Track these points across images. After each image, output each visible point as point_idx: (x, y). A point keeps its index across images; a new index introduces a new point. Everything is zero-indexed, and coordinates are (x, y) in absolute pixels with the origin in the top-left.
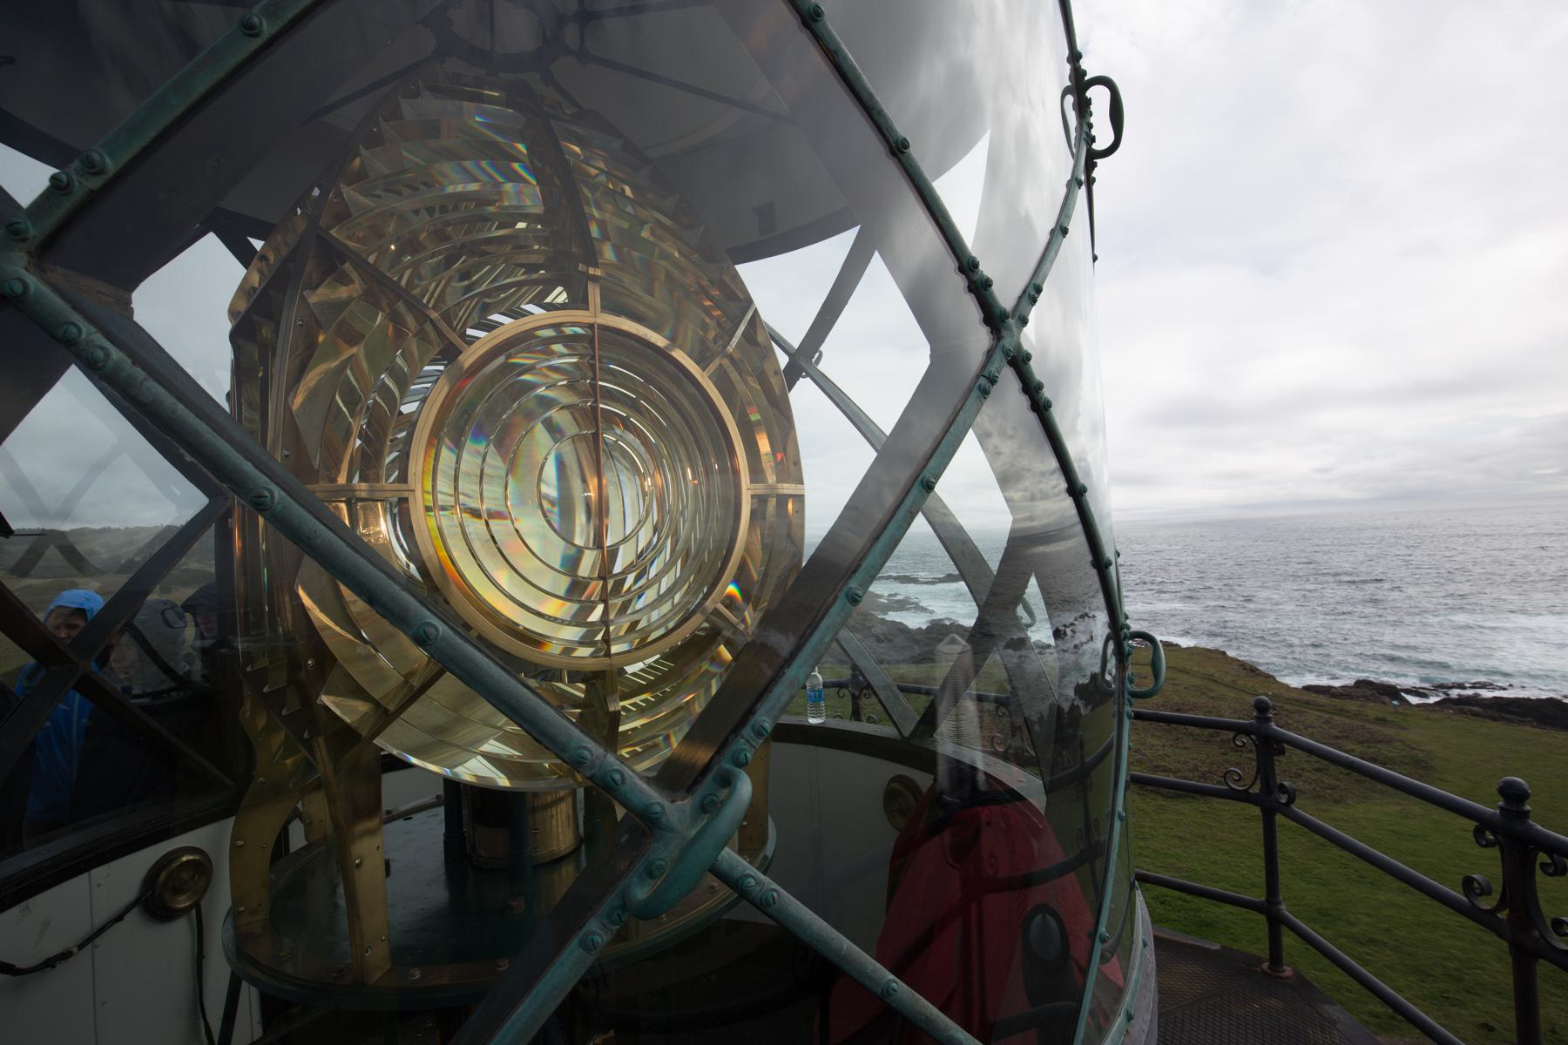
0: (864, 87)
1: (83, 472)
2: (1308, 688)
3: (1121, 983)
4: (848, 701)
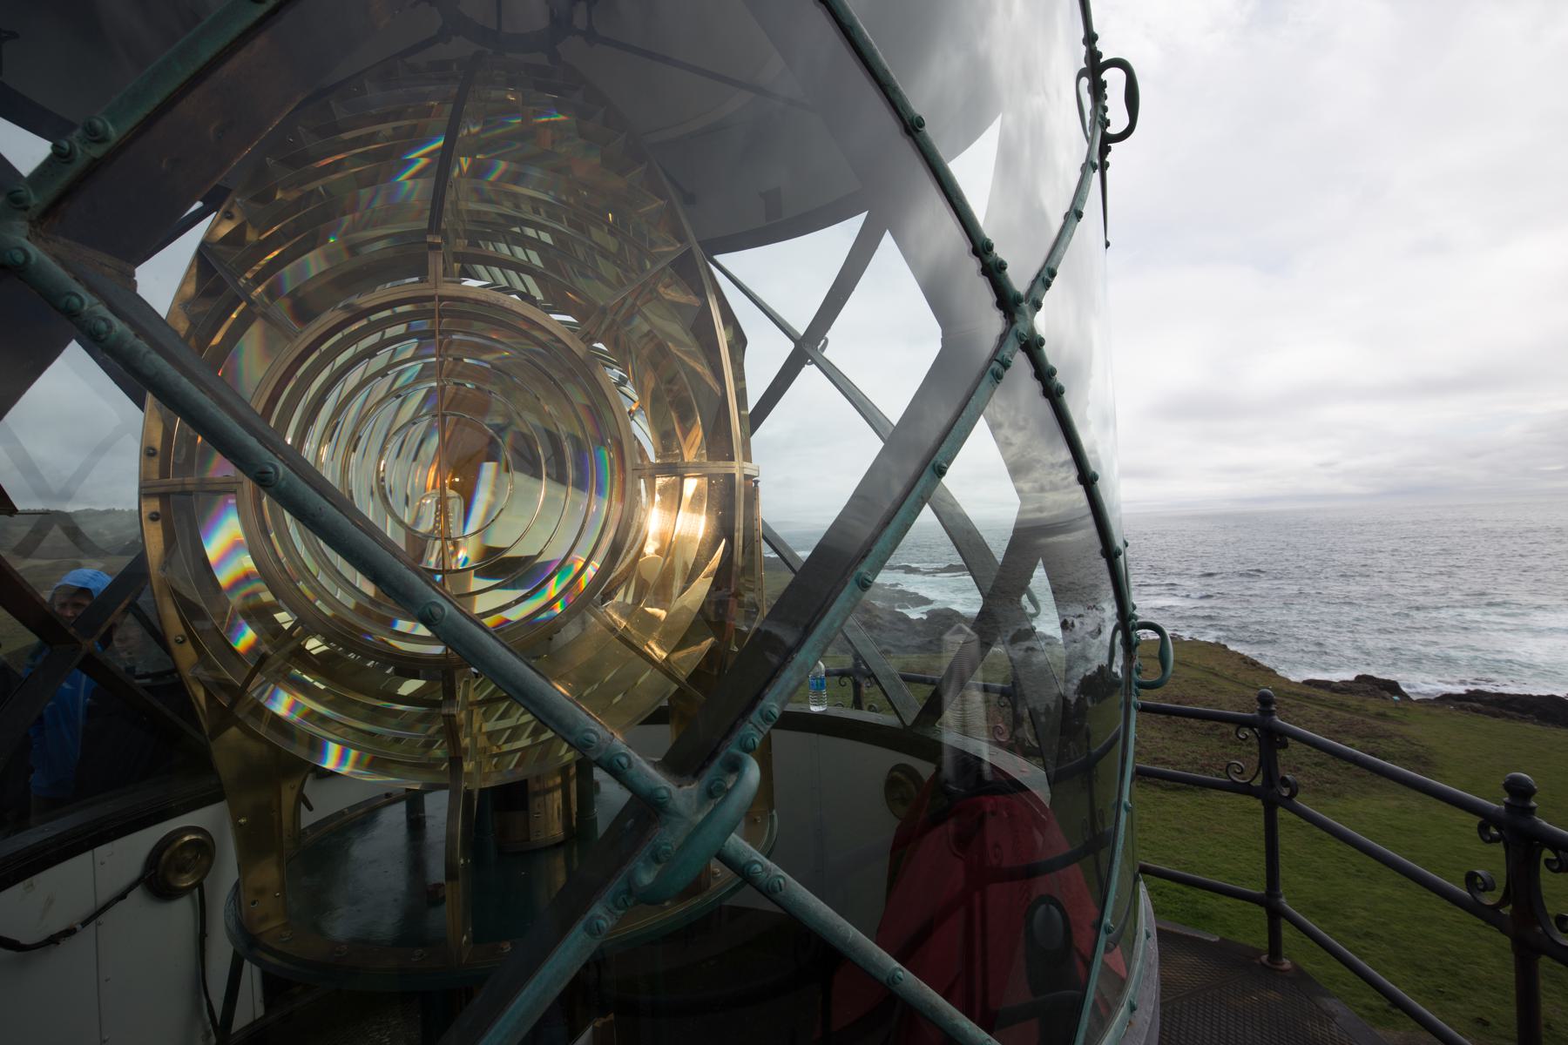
0: (880, 64)
1: (77, 436)
2: (1309, 683)
3: (1124, 974)
4: (849, 689)
